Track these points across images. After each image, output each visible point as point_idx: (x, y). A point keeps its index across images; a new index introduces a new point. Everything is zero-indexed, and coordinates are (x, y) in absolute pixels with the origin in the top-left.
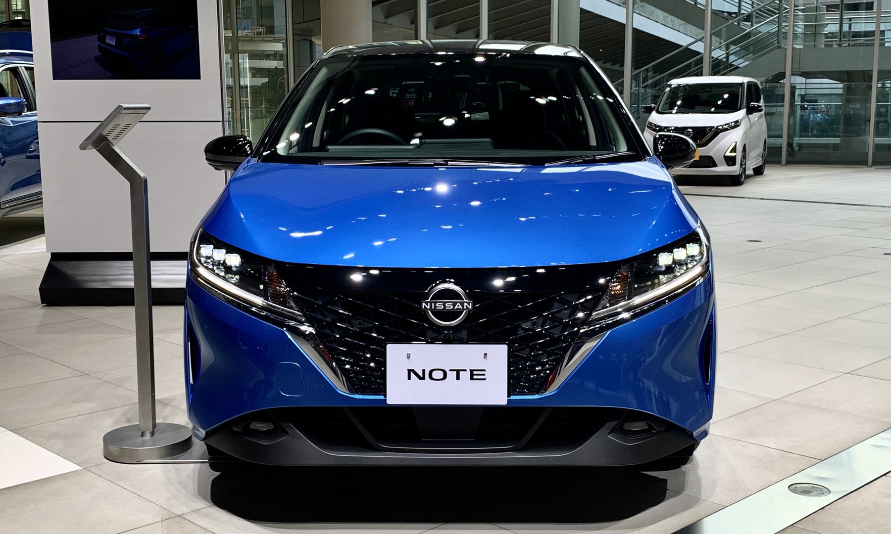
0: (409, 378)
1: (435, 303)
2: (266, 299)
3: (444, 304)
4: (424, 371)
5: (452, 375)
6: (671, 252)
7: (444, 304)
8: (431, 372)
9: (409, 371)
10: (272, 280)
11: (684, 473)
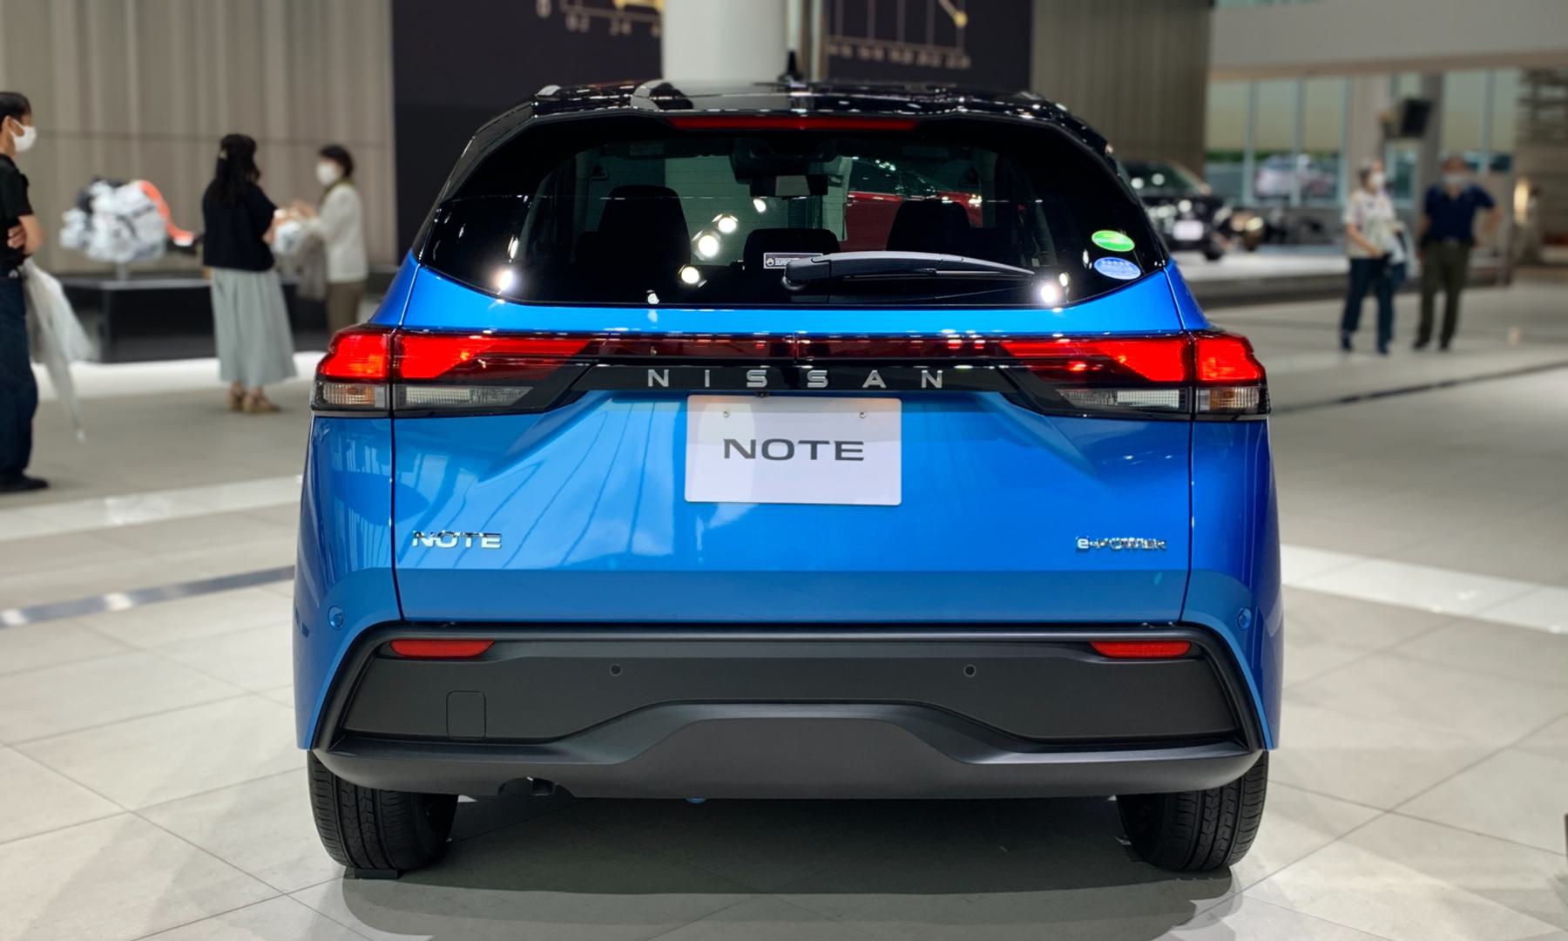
0: (727, 455)
5: (827, 452)
6: (1356, 263)
9: (728, 443)
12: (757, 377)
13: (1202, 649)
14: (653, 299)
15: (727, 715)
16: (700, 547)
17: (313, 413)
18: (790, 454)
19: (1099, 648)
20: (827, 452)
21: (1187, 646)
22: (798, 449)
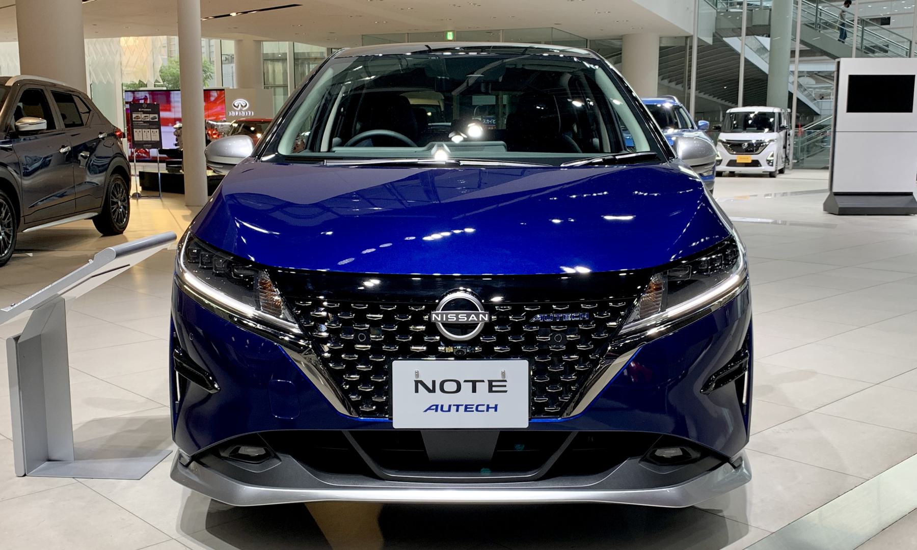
0: (417, 391)
1: (447, 315)
2: (258, 309)
3: (457, 315)
4: (434, 382)
7: (457, 315)
9: (417, 382)
10: (265, 288)
13: (113, 173)
14: (632, 365)
16: (373, 250)
18: (459, 389)
22: (463, 385)
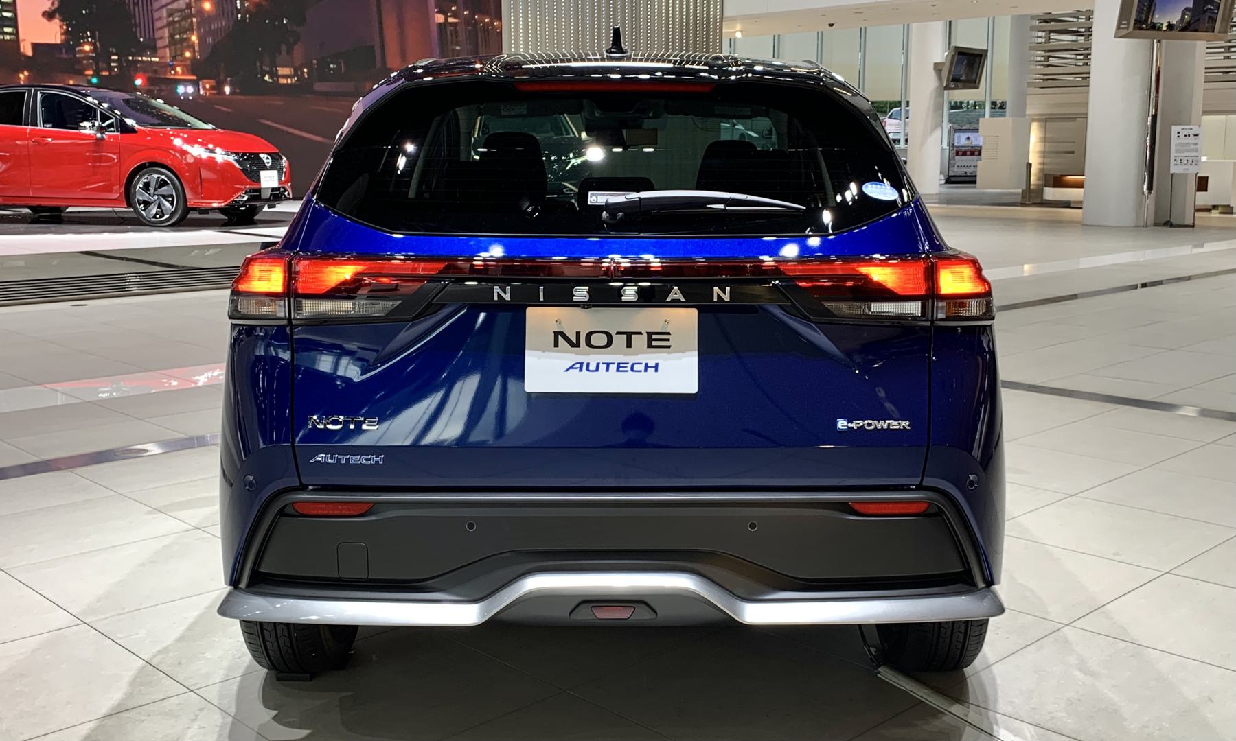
0: (556, 345)
4: (578, 334)
5: (613, 368)
8: (589, 335)
9: (557, 334)
11: (984, 655)
12: (581, 293)
15: (314, 618)
17: (230, 321)
19: (857, 507)
20: (613, 368)
21: (925, 505)
